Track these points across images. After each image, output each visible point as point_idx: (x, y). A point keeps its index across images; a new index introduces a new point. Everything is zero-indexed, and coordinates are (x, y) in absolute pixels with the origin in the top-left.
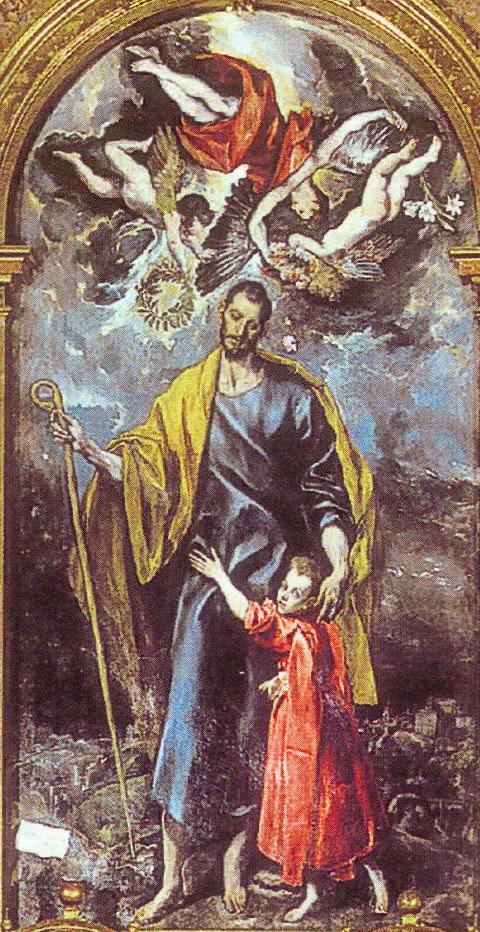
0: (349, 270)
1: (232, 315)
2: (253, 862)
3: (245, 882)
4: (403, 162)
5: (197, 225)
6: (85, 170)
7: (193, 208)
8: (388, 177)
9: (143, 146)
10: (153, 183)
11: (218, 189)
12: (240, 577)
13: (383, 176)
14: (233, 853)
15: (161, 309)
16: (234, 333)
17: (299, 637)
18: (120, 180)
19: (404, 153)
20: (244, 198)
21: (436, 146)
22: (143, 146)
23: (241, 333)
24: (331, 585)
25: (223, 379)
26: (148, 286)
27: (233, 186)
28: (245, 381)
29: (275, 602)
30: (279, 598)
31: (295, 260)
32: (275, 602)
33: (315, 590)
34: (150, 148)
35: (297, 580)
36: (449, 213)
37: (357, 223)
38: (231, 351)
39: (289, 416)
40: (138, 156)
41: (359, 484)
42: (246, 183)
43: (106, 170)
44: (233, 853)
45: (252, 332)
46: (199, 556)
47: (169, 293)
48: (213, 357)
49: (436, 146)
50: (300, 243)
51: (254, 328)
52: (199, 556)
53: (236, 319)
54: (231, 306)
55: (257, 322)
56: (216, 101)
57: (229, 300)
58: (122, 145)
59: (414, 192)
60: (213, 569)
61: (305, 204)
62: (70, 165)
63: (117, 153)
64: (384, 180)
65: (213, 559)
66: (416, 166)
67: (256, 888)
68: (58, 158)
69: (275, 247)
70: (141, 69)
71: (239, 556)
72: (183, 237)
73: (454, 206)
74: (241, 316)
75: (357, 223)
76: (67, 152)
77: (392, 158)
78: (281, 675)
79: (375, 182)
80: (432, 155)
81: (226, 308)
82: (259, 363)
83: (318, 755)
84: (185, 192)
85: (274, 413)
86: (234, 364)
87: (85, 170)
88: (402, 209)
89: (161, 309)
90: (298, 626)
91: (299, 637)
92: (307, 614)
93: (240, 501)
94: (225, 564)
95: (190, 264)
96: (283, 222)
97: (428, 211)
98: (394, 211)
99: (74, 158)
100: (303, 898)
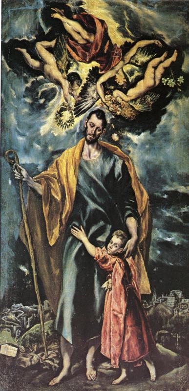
0: (138, 107)
1: (90, 124)
2: (100, 358)
3: (95, 369)
4: (161, 62)
5: (76, 87)
6: (28, 56)
7: (74, 78)
8: (155, 68)
9: (53, 43)
10: (57, 65)
11: (84, 70)
12: (93, 240)
13: (153, 67)
14: (89, 357)
15: (64, 121)
16: (90, 133)
17: (117, 264)
18: (43, 62)
19: (162, 58)
20: (94, 75)
21: (175, 54)
22: (53, 43)
23: (93, 133)
24: (131, 242)
25: (84, 153)
26: (60, 113)
27: (90, 70)
28: (94, 155)
29: (106, 248)
30: (108, 247)
31: (116, 103)
32: (106, 248)
33: (123, 246)
34: (56, 44)
35: (116, 240)
36: (179, 82)
37: (141, 87)
38: (89, 141)
39: (112, 170)
40: (49, 49)
41: (143, 199)
42: (95, 69)
43: (36, 56)
44: (89, 357)
45: (98, 133)
46: (75, 230)
47: (67, 115)
48: (80, 143)
49: (175, 54)
50: (117, 93)
51: (99, 131)
52: (75, 230)
53: (92, 127)
54: (90, 121)
55: (101, 128)
56: (84, 34)
57: (89, 118)
58: (43, 44)
59: (166, 74)
60: (81, 235)
61: (121, 80)
62: (21, 54)
63: (41, 47)
64: (153, 69)
65: (81, 230)
66: (167, 63)
67: (101, 370)
68: (17, 50)
69: (107, 97)
70: (55, 17)
71: (93, 229)
72: (71, 91)
73: (181, 80)
74: (94, 125)
75: (141, 87)
76: (21, 48)
77: (157, 60)
78: (110, 280)
79: (149, 71)
80: (173, 58)
81: (88, 121)
82: (100, 148)
83: (126, 315)
84: (70, 71)
85: (47, 127)
86: (90, 146)
87: (28, 56)
88: (161, 80)
89: (64, 121)
90: (116, 260)
91: (117, 264)
92: (120, 255)
93: (92, 205)
94: (87, 233)
95: (72, 102)
96: (110, 86)
97: (171, 83)
98: (157, 82)
99: (24, 51)
100: (120, 374)
